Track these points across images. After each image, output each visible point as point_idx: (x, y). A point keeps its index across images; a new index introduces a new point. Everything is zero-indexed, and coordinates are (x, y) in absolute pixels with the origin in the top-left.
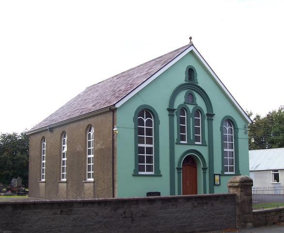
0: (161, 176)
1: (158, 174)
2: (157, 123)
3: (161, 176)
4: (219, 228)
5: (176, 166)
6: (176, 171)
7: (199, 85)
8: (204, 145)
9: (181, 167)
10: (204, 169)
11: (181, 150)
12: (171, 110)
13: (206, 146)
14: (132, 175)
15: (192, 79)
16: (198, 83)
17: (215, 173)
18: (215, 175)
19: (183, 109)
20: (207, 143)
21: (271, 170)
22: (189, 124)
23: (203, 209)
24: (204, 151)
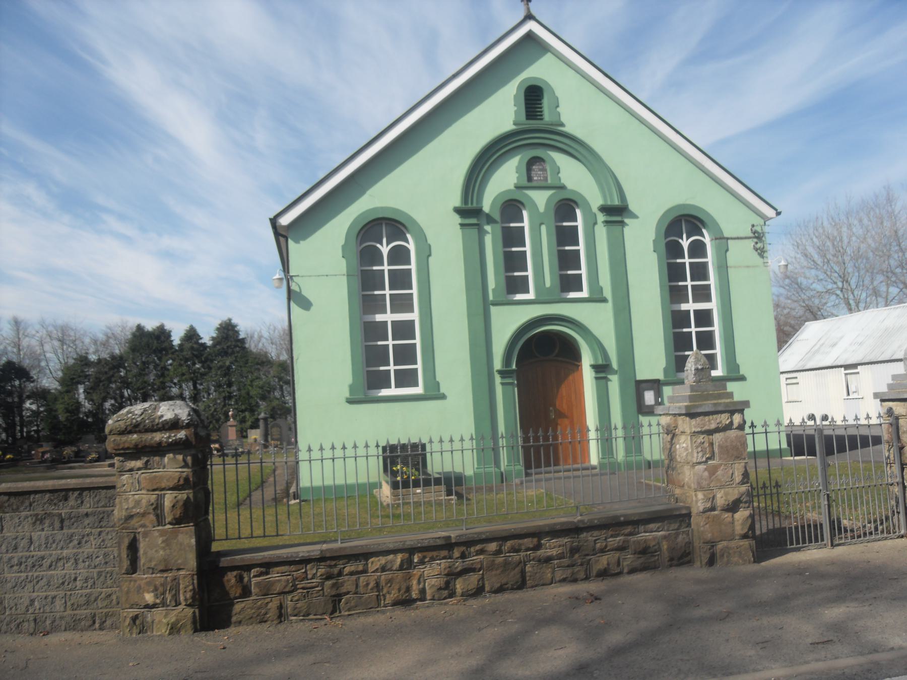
0: (443, 397)
1: (434, 394)
2: (425, 252)
3: (443, 397)
4: (582, 575)
5: (498, 364)
6: (498, 379)
7: (568, 129)
8: (597, 298)
9: (514, 367)
10: (602, 369)
11: (507, 322)
12: (470, 213)
13: (604, 300)
14: (344, 400)
15: (230, 320)
16: (562, 125)
17: (640, 377)
18: (639, 383)
19: (511, 207)
20: (608, 293)
21: (841, 366)
22: (538, 245)
23: (192, 641)
24: (599, 320)
